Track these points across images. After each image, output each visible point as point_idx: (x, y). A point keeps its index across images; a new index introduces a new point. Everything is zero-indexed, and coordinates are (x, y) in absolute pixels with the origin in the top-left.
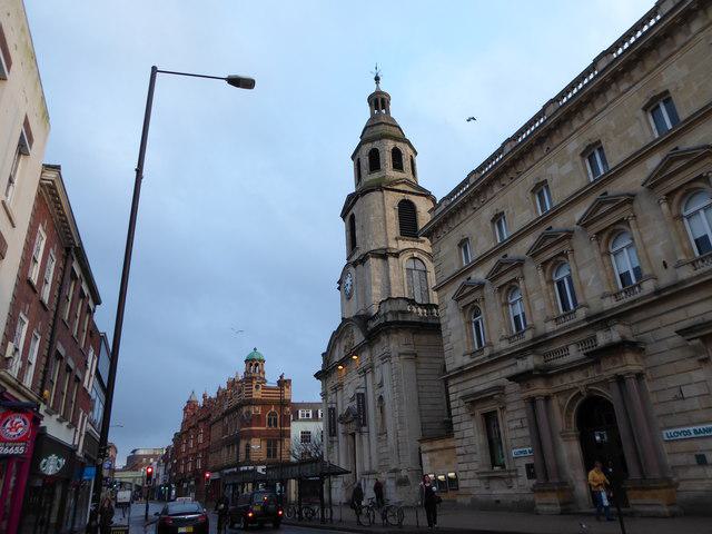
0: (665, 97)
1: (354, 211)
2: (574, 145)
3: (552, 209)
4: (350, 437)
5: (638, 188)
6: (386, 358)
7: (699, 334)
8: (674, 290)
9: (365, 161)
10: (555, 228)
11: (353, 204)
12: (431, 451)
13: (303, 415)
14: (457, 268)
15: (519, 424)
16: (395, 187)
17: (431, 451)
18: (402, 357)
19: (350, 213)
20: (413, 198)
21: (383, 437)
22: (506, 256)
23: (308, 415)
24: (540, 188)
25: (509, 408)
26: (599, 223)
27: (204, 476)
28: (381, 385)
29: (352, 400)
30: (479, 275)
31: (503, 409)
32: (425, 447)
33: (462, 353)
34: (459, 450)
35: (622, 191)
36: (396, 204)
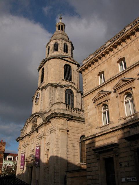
0: (123, 59)
1: (44, 66)
2: (115, 59)
3: (101, 84)
4: (30, 169)
5: (136, 77)
6: (52, 131)
7: (97, 151)
8: (116, 128)
9: (52, 47)
10: (104, 90)
11: (44, 63)
12: (71, 177)
13: (9, 159)
14: (95, 86)
15: (127, 164)
16: (64, 59)
17: (71, 177)
18: (61, 131)
19: (42, 68)
20: (71, 64)
21: (47, 169)
22: (103, 90)
23: (11, 159)
24: (121, 61)
25: (121, 156)
26: (99, 101)
27: (7, 175)
28: (48, 144)
29: (33, 151)
30: (108, 88)
31: (117, 156)
32: (68, 175)
33: (96, 127)
34: (88, 178)
35: (130, 77)
36: (64, 65)
